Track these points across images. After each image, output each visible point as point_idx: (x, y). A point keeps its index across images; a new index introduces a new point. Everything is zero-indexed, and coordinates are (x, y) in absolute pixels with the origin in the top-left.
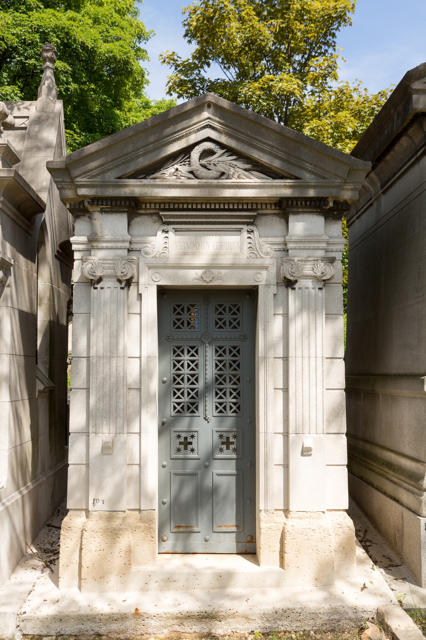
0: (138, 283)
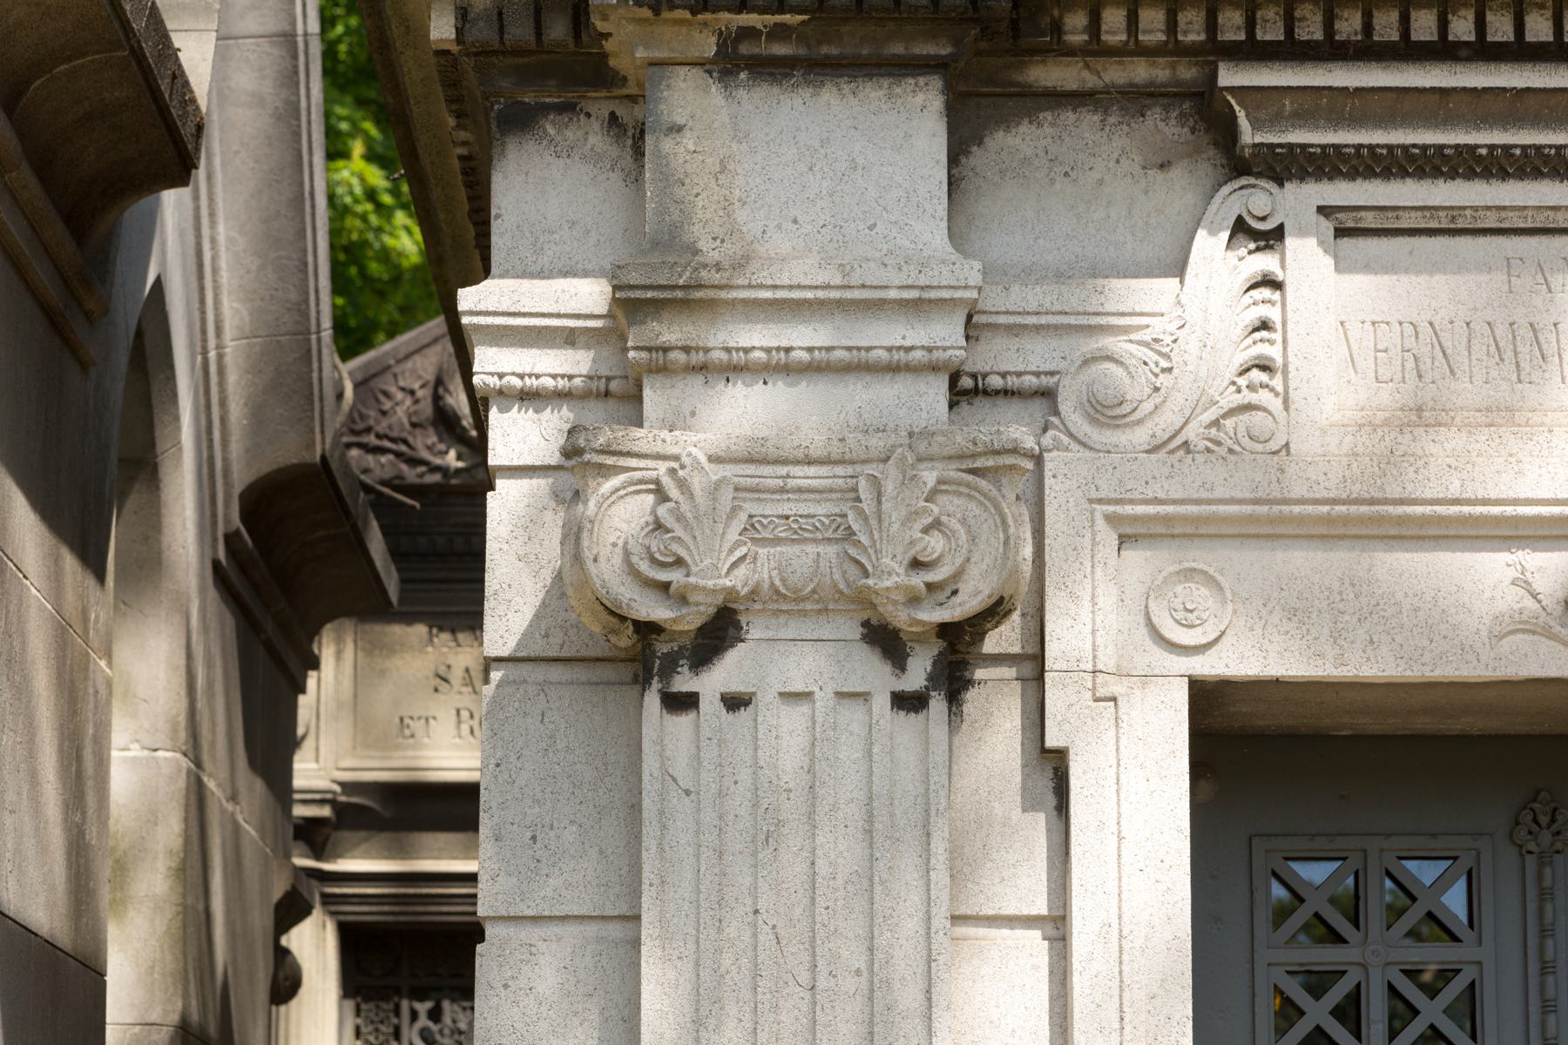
0: (1033, 666)
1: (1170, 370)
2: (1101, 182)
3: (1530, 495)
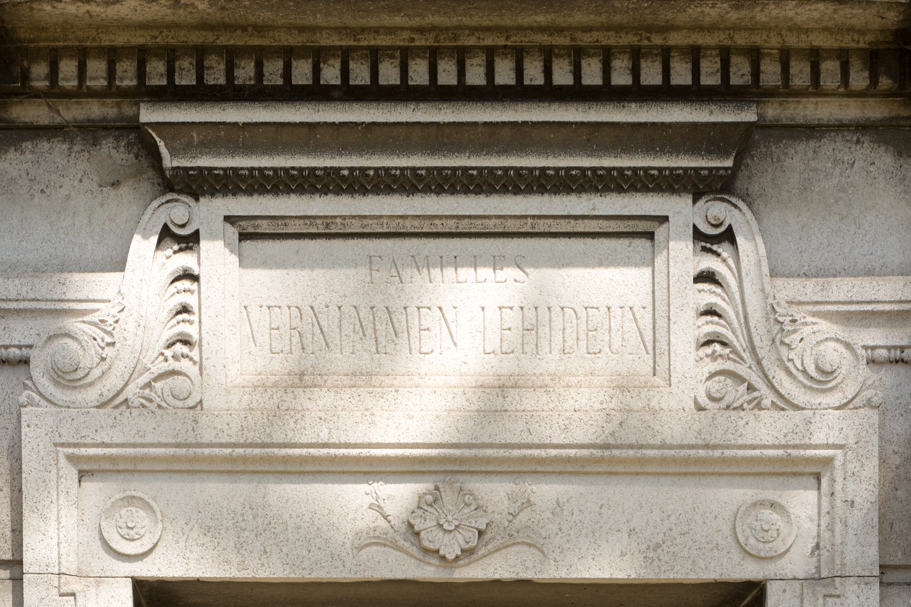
1: (113, 344)
2: (68, 197)
3: (380, 440)
